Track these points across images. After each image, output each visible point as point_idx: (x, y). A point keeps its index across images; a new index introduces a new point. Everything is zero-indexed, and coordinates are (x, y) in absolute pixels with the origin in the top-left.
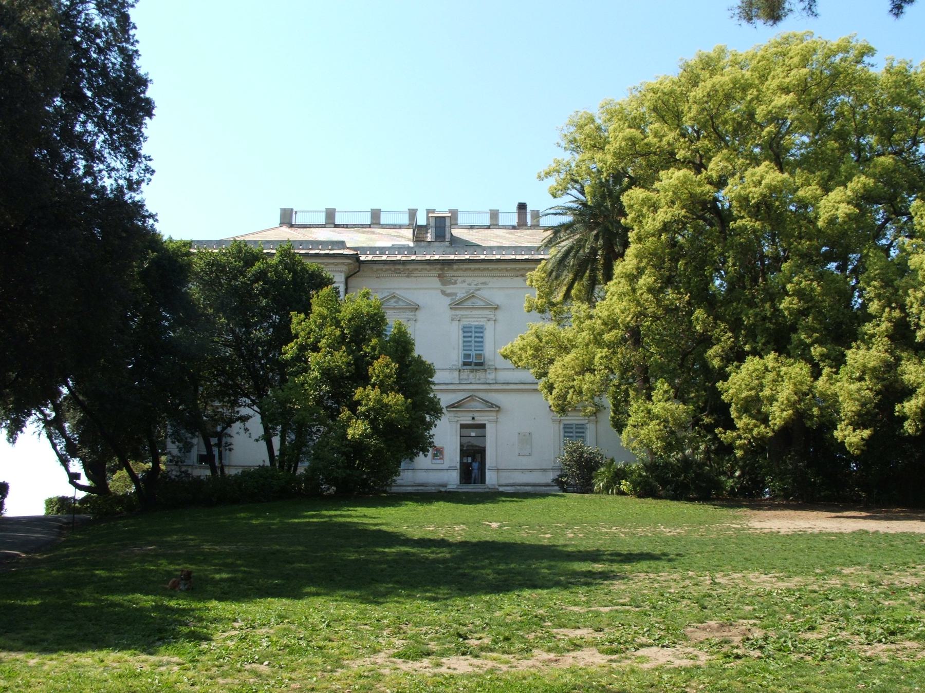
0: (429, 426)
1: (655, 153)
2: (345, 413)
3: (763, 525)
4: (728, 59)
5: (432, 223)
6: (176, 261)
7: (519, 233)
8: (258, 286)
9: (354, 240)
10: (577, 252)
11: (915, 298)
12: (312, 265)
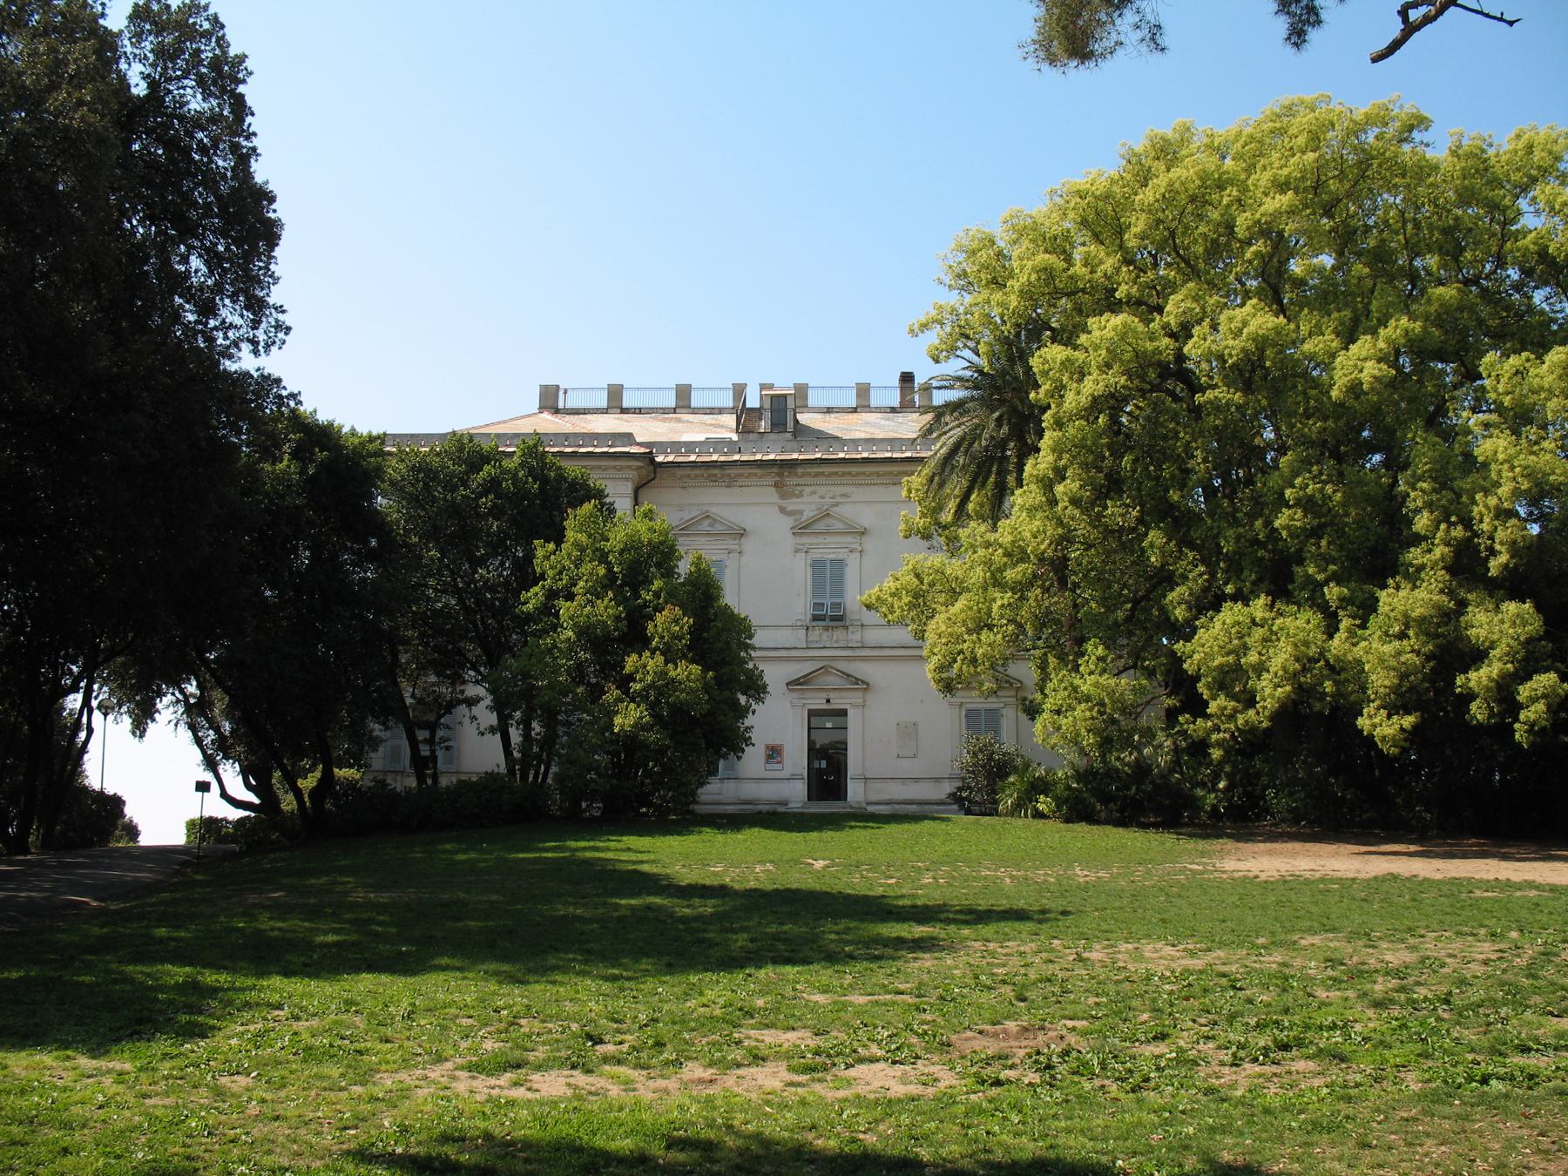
0: (743, 712)
1: (1083, 290)
2: (613, 693)
3: (1242, 866)
4: (1198, 141)
5: (767, 405)
6: (358, 464)
7: (900, 417)
8: (486, 502)
9: (647, 431)
10: (971, 445)
11: (1486, 506)
12: (572, 469)
